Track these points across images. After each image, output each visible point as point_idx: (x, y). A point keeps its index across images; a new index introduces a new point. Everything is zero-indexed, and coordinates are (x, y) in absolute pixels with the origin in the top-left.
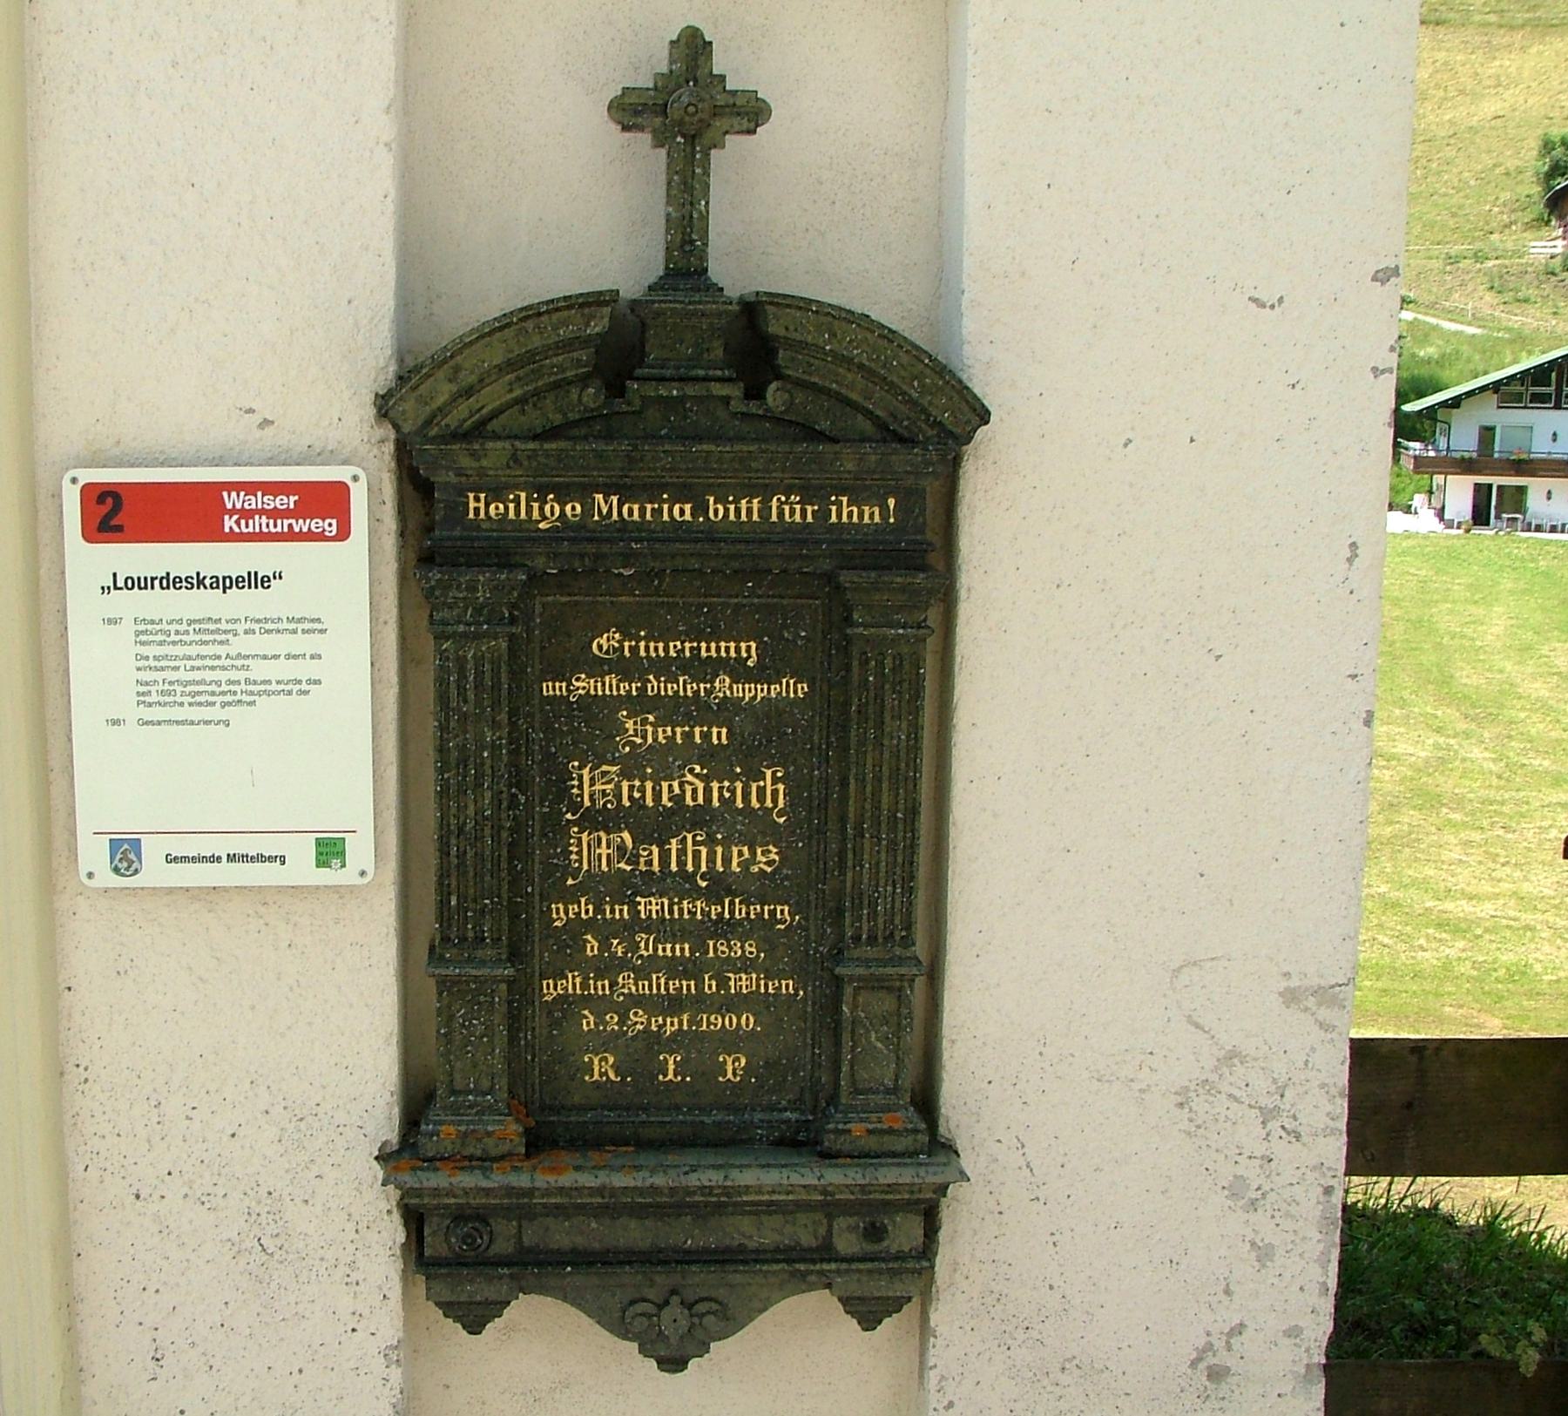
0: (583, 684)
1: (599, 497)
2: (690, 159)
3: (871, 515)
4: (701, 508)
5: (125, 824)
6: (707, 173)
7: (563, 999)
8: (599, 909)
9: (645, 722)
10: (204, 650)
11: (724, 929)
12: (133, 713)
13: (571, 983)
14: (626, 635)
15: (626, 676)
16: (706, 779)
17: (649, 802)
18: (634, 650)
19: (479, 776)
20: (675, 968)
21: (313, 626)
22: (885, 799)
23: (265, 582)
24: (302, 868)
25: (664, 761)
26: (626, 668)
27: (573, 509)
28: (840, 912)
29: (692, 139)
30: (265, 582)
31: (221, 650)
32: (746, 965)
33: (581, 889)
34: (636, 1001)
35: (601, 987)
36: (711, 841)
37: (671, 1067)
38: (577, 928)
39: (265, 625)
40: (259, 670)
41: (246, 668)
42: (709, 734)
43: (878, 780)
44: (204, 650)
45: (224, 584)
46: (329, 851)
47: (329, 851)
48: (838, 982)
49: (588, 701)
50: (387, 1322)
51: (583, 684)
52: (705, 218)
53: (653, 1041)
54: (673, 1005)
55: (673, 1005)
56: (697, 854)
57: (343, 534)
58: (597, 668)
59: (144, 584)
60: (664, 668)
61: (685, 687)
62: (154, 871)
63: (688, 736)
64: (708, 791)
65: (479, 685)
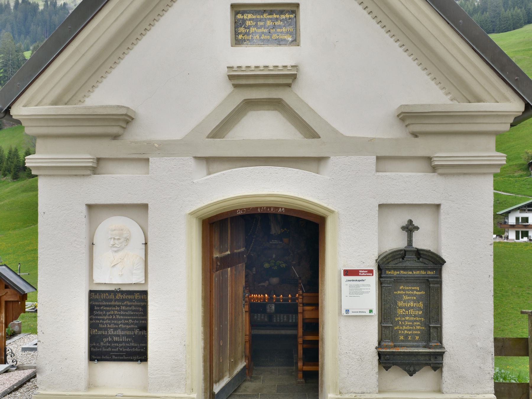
0: (399, 292)
1: (401, 271)
2: (411, 234)
3: (432, 273)
4: (413, 272)
5: (347, 308)
6: (412, 235)
7: (397, 329)
8: (401, 319)
9: (406, 296)
10: (357, 288)
11: (416, 321)
12: (348, 295)
13: (398, 328)
14: (404, 287)
15: (404, 291)
16: (413, 303)
17: (103, 334)
18: (405, 288)
19: (388, 303)
20: (410, 326)
21: (369, 285)
22: (435, 306)
23: (364, 281)
24: (368, 313)
25: (408, 301)
26: (404, 290)
27: (398, 273)
28: (430, 319)
29: (411, 231)
30: (364, 281)
31: (359, 288)
32: (419, 325)
33: (399, 316)
34: (406, 329)
35: (401, 328)
36: (414, 310)
37: (410, 338)
38: (398, 321)
39: (363, 285)
40: (363, 291)
41: (362, 290)
42: (411, 298)
43: (434, 303)
44: (357, 288)
45: (359, 281)
46: (371, 311)
47: (371, 311)
48: (430, 327)
49: (399, 294)
50: (376, 369)
51: (399, 292)
52: (412, 240)
53: (408, 334)
54: (410, 330)
55: (410, 330)
56: (412, 312)
57: (373, 275)
58: (400, 290)
59: (350, 281)
60: (408, 290)
61: (411, 292)
62: (351, 314)
63: (411, 298)
64: (413, 304)
65: (388, 292)
